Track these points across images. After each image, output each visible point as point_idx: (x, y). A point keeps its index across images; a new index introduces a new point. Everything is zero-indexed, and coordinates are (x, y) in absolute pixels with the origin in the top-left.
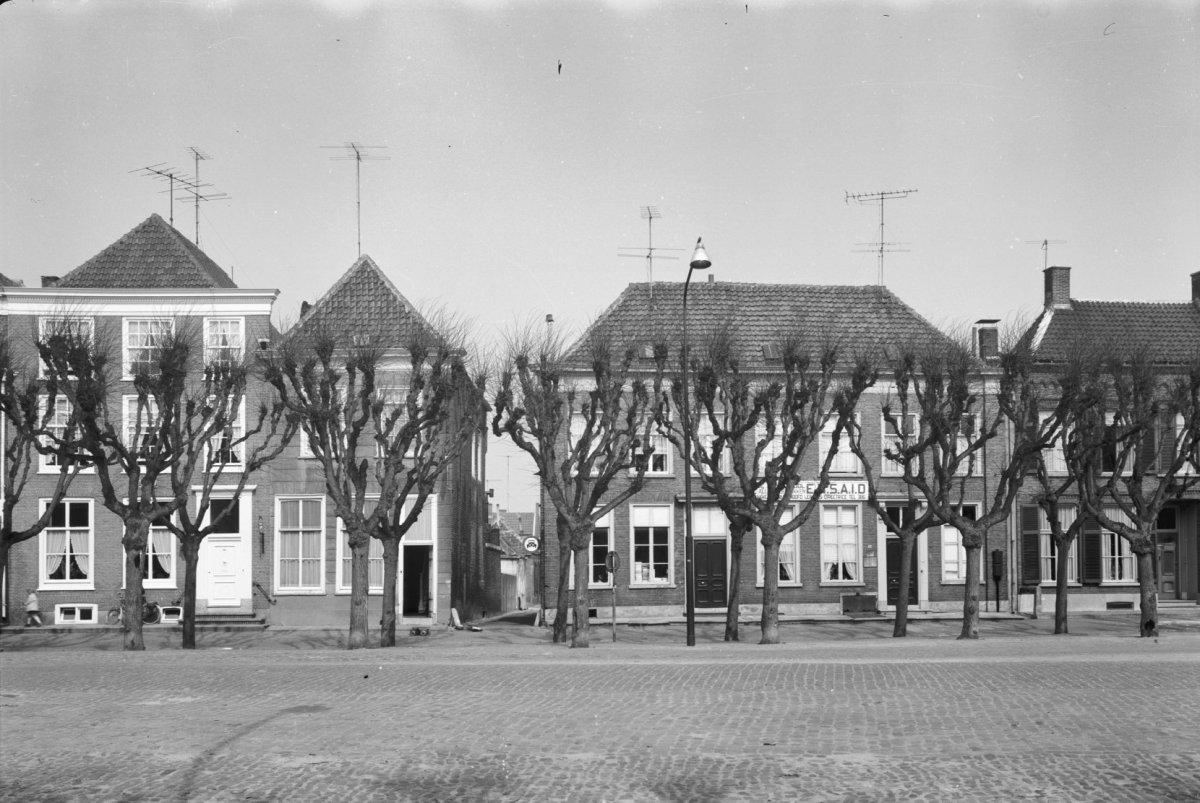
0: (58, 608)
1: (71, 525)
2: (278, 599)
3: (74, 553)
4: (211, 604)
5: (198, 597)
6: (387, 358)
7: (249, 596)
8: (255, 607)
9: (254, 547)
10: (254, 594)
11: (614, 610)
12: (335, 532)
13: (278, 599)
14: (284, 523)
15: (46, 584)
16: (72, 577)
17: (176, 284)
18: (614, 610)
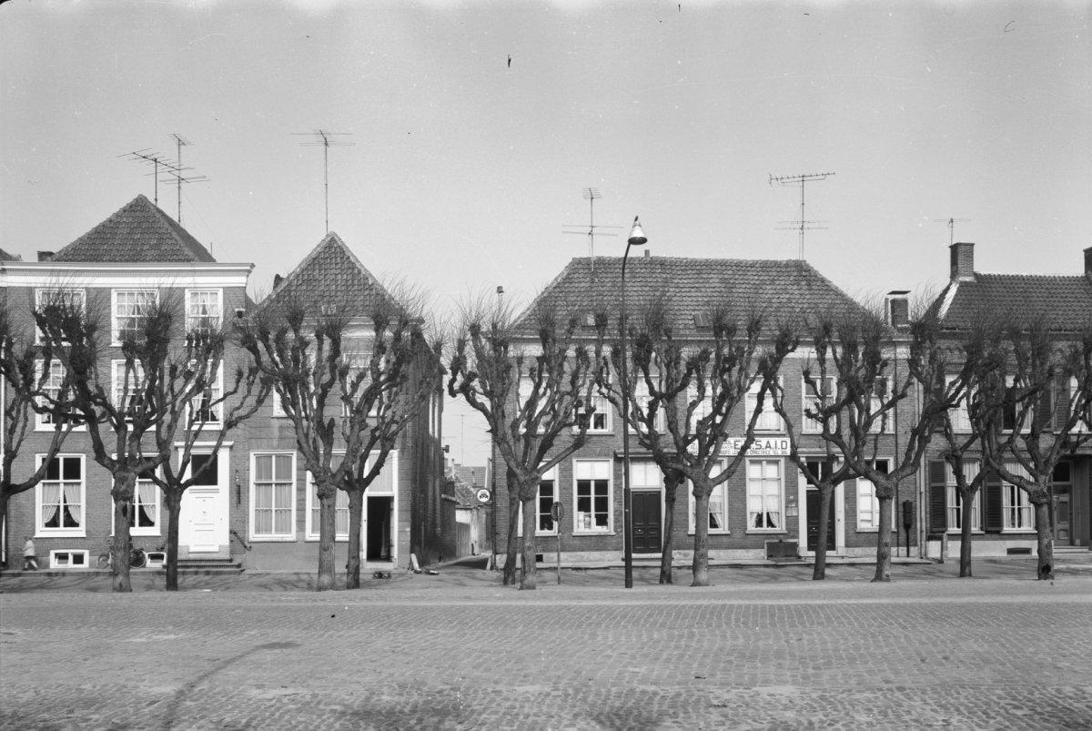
0: (52, 553)
1: (65, 478)
2: (253, 545)
3: (68, 504)
4: (192, 549)
5: (180, 544)
6: (352, 326)
7: (227, 543)
8: (232, 552)
9: (231, 498)
10: (232, 541)
11: (559, 556)
12: (305, 484)
13: (253, 545)
14: (259, 476)
15: (42, 532)
16: (65, 526)
17: (160, 259)
18: (559, 556)
